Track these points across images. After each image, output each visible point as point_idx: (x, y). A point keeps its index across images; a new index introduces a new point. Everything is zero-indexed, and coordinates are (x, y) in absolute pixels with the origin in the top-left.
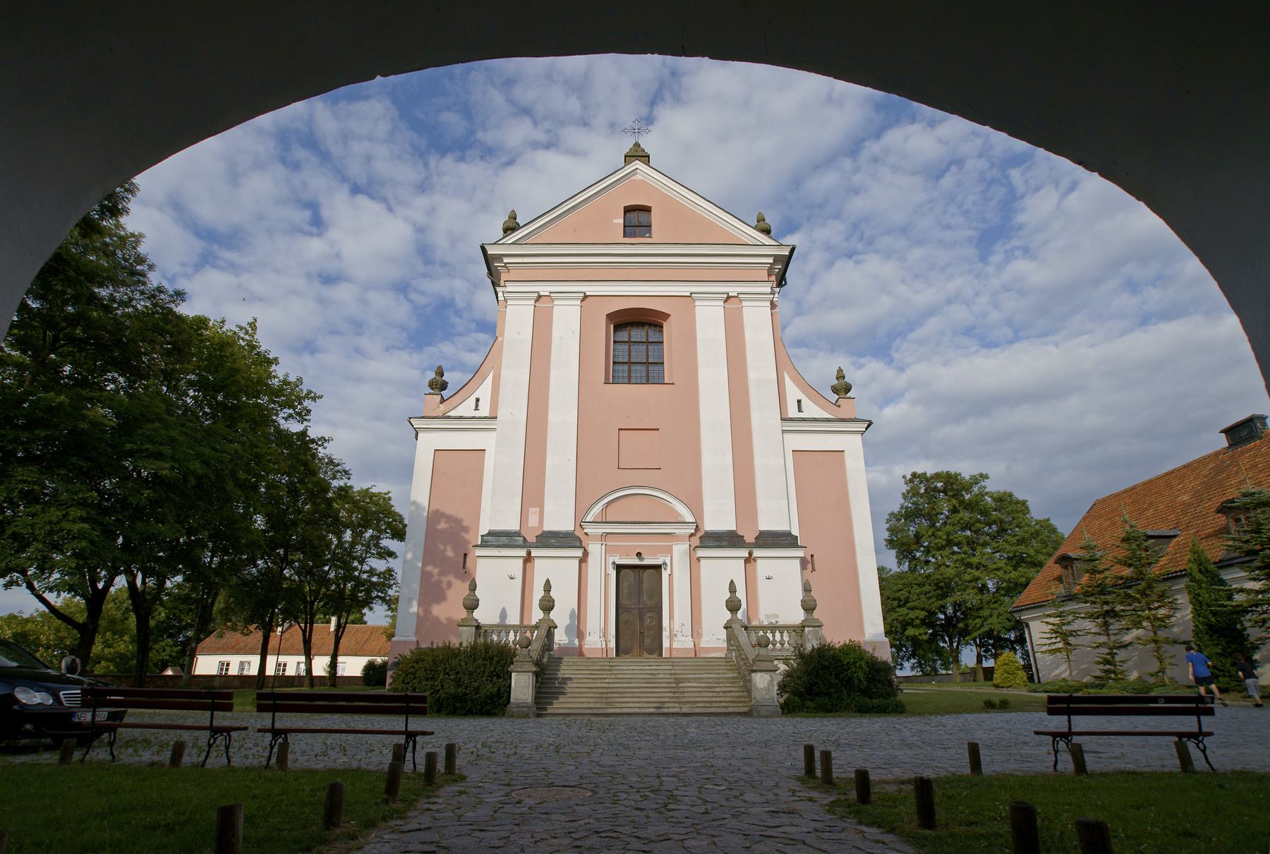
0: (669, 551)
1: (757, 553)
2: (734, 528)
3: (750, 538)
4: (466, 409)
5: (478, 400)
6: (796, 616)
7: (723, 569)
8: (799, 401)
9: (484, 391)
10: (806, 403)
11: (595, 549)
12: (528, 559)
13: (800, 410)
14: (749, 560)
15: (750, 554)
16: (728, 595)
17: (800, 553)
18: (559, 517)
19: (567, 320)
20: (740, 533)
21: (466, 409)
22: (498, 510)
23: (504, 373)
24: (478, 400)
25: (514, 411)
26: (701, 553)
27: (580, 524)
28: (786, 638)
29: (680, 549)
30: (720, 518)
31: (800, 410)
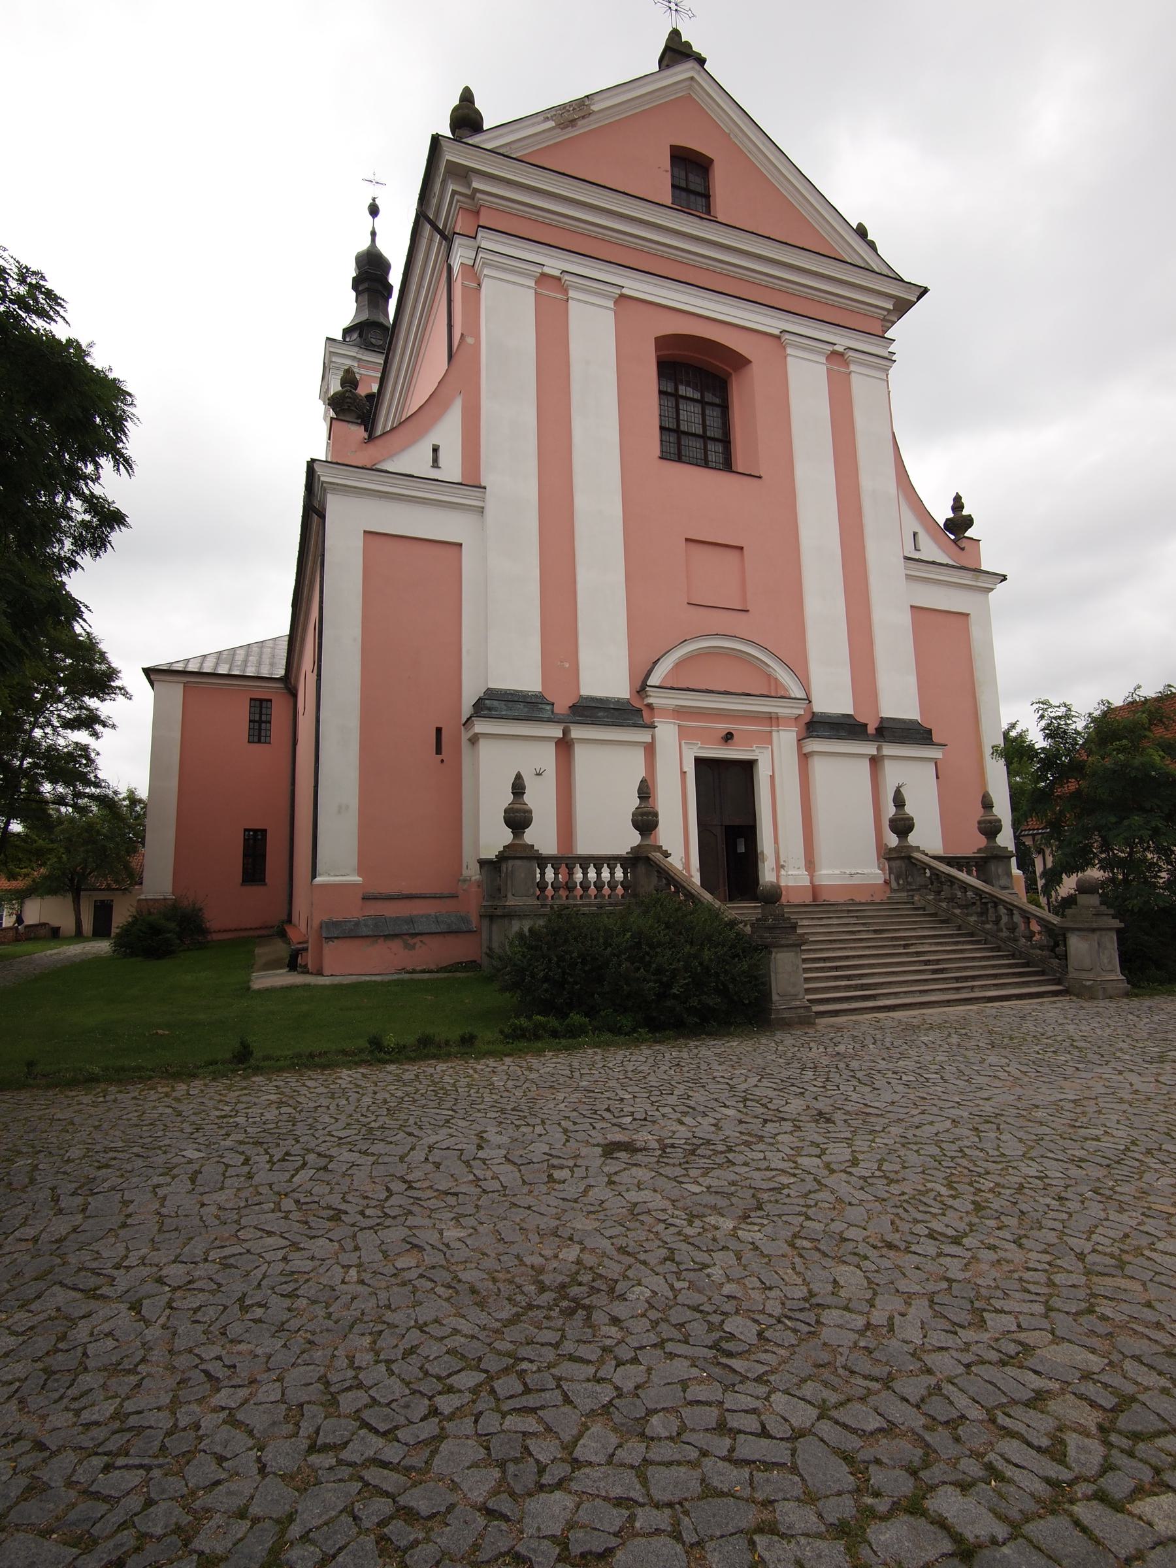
0: (767, 739)
1: (576, 732)
2: (850, 711)
3: (562, 706)
4: (414, 460)
5: (435, 450)
6: (627, 840)
7: (842, 776)
8: (915, 534)
9: (448, 431)
10: (923, 538)
11: (666, 733)
12: (565, 746)
13: (435, 463)
14: (565, 746)
15: (566, 732)
16: (510, 797)
17: (936, 753)
18: (605, 674)
19: (593, 333)
20: (861, 719)
21: (414, 460)
22: (507, 656)
23: (487, 405)
24: (435, 450)
25: (513, 479)
26: (814, 745)
27: (642, 689)
28: (619, 874)
29: (786, 738)
30: (833, 698)
31: (435, 463)
